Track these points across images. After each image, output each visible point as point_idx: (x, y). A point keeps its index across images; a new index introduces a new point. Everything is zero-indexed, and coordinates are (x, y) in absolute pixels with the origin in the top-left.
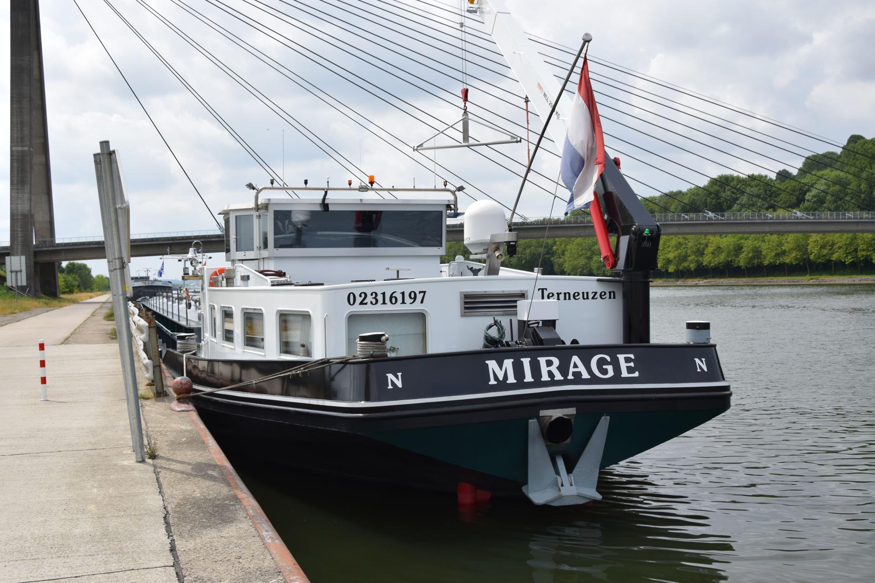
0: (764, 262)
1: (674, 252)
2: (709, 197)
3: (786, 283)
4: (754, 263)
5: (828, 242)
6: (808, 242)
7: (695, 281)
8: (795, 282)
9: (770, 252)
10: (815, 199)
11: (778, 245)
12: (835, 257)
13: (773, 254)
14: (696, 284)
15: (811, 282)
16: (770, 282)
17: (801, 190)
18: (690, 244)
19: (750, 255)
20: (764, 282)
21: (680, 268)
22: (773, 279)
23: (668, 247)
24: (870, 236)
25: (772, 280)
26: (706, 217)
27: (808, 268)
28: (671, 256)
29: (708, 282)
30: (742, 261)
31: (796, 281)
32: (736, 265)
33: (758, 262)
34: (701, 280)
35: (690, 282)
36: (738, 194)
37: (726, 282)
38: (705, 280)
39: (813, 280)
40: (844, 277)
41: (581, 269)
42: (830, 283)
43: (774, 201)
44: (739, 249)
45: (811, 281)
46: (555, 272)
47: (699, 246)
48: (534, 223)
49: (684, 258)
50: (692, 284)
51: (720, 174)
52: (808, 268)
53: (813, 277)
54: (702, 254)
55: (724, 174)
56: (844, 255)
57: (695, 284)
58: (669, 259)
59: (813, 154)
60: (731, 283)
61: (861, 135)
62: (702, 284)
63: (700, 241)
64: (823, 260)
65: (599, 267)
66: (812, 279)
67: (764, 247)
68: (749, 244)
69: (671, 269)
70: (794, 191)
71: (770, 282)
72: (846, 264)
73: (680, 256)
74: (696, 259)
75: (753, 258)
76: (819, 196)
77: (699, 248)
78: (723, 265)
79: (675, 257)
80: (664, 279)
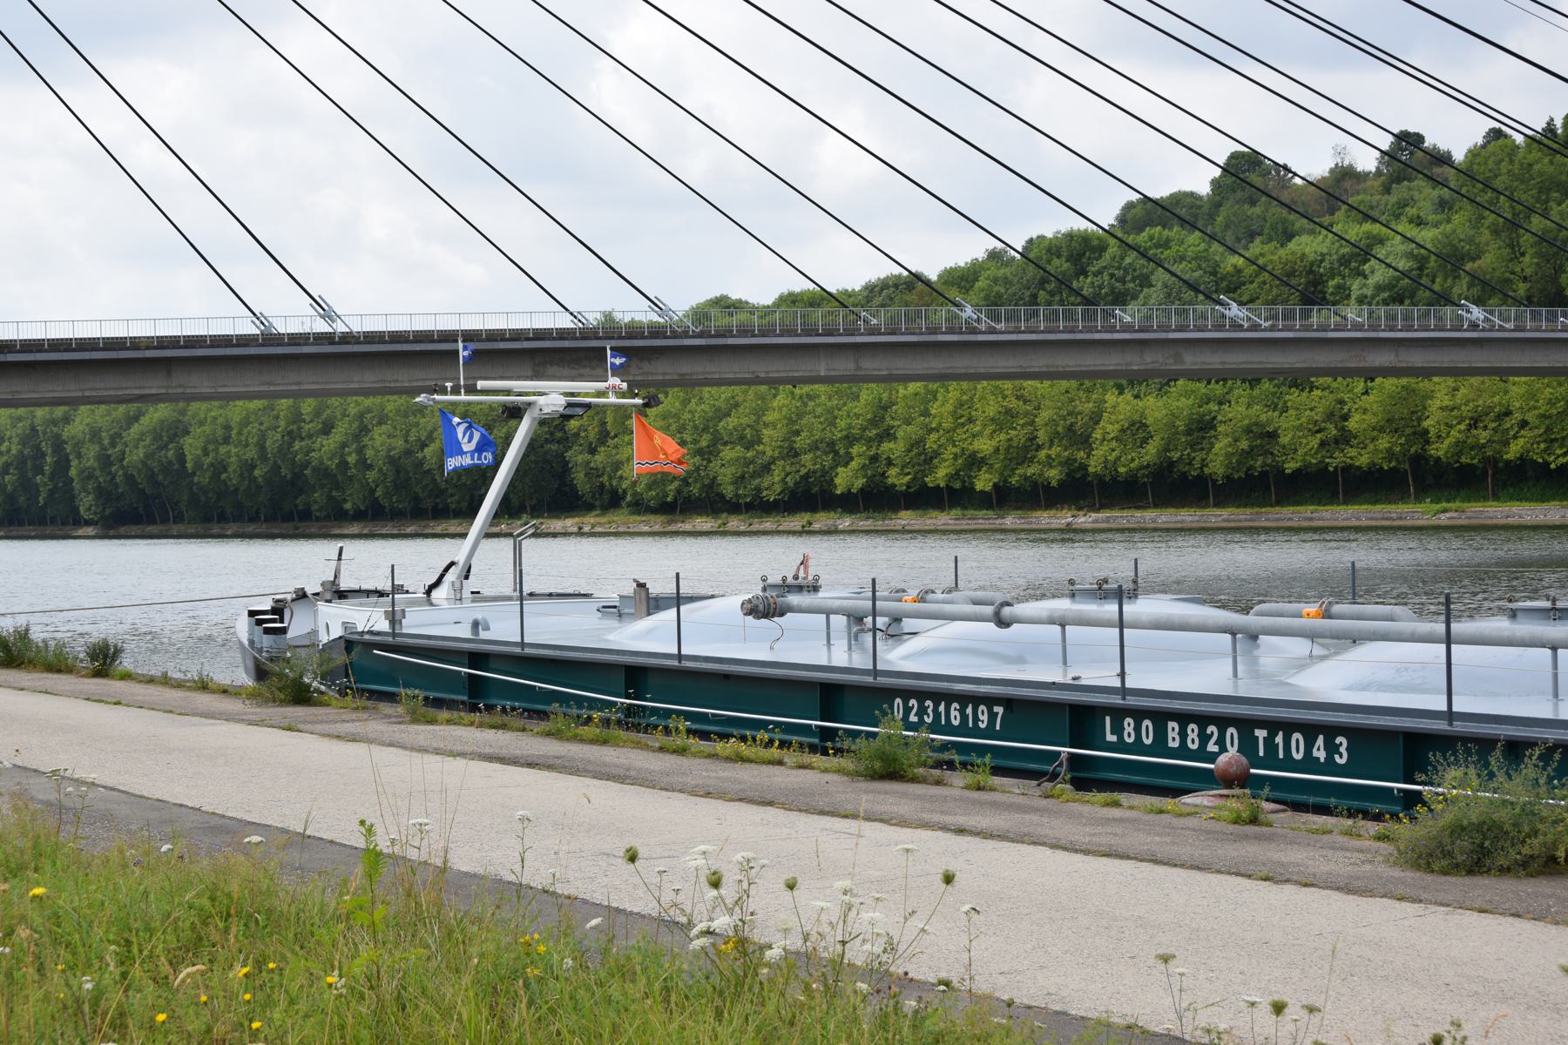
0: (1286, 466)
1: (991, 437)
2: (1044, 289)
3: (1364, 523)
4: (1251, 468)
5: (1491, 408)
6: (867, 462)
7: (1064, 517)
8: (1391, 519)
9: (1306, 437)
10: (1386, 295)
11: (1330, 416)
12: (1513, 451)
13: (1315, 442)
14: (1068, 524)
15: (1444, 519)
16: (1311, 519)
17: (1311, 272)
18: (1045, 415)
19: (1244, 445)
20: (1291, 519)
21: (1014, 480)
22: (1316, 511)
23: (971, 420)
24: (1548, 390)
25: (1314, 515)
26: (1224, 316)
27: (1411, 483)
28: (984, 446)
29: (1108, 520)
30: (1218, 458)
31: (1394, 515)
32: (1195, 473)
33: (1264, 464)
34: (1081, 513)
35: (1046, 518)
36: (1130, 282)
37: (1164, 518)
38: (1094, 515)
39: (1448, 515)
40: (1545, 506)
41: (676, 484)
42: (1503, 521)
43: (40, 471)
44: (1202, 428)
45: (1443, 516)
46: (578, 498)
47: (1071, 420)
48: (673, 332)
49: (1025, 452)
50: (1053, 526)
51: (1064, 228)
52: (1411, 483)
53: (1444, 505)
54: (1085, 442)
55: (1075, 228)
56: (1543, 446)
57: (1063, 527)
58: (974, 453)
59: (1082, 225)
60: (1183, 521)
61: (1188, 188)
62: (1089, 526)
63: (1075, 407)
64: (1472, 459)
65: (743, 477)
66: (1445, 511)
67: (1287, 426)
68: (1241, 409)
69: (984, 482)
70: (1291, 274)
71: (1311, 519)
72: (1550, 470)
73: (1010, 446)
74: (1066, 453)
75: (1250, 453)
76: (1394, 286)
77: (1072, 425)
78: (1150, 473)
79: (997, 450)
80: (957, 512)
